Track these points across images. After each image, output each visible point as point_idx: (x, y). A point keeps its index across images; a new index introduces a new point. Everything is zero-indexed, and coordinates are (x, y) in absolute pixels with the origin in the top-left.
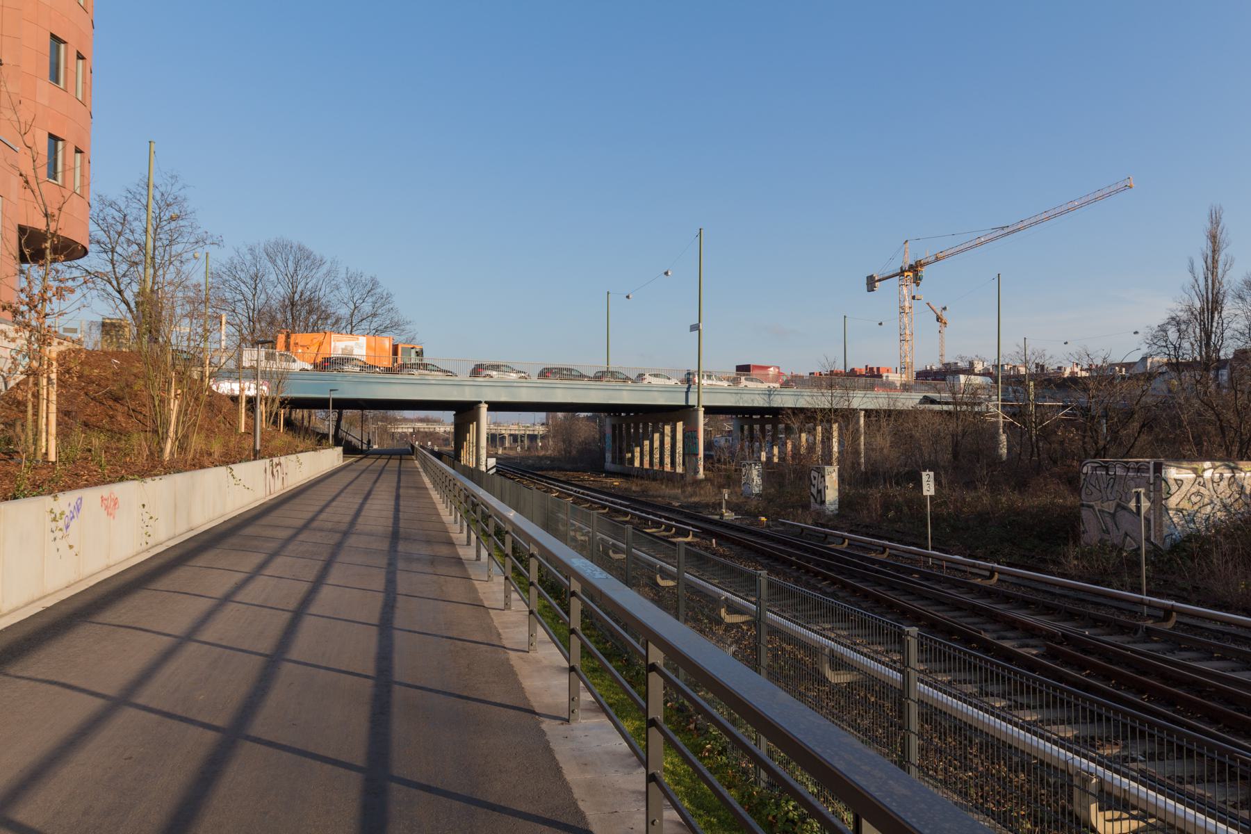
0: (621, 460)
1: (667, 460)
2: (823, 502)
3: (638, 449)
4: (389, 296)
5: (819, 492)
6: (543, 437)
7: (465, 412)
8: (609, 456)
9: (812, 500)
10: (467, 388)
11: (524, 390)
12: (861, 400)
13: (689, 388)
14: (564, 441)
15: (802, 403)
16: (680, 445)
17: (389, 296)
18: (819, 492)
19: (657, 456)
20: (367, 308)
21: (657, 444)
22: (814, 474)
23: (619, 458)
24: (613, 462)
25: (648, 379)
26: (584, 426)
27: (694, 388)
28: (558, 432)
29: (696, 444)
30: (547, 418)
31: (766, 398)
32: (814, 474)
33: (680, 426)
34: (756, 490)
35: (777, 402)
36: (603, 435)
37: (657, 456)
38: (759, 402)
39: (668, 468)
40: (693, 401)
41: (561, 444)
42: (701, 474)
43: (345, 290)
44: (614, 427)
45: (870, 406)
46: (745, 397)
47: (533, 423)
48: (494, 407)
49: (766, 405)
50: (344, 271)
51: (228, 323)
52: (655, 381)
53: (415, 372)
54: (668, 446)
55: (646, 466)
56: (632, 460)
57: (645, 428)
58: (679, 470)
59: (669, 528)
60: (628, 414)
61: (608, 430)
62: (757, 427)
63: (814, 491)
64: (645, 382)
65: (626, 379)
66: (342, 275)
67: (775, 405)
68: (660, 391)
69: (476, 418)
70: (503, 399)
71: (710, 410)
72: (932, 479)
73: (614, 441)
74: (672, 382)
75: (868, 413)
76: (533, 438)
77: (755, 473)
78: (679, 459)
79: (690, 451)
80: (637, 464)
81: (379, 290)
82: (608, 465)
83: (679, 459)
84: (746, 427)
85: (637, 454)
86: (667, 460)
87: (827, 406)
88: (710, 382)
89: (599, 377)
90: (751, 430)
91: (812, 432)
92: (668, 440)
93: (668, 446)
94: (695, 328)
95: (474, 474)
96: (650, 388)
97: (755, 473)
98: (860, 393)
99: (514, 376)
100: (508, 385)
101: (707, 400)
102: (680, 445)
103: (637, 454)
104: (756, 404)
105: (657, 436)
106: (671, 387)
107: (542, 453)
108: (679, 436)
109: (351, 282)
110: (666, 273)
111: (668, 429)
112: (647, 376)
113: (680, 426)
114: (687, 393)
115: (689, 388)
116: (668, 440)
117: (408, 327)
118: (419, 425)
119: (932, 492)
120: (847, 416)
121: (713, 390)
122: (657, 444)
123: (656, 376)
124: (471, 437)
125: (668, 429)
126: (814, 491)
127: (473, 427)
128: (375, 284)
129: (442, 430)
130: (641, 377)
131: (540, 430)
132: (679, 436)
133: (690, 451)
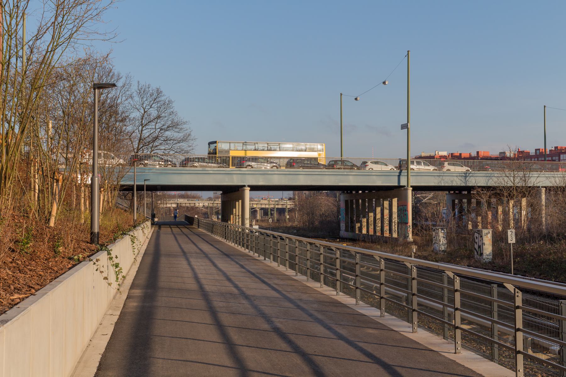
0: (353, 228)
1: (386, 228)
2: (482, 254)
3: (365, 220)
4: (170, 102)
5: (479, 247)
6: (290, 211)
7: (231, 194)
8: (343, 226)
9: (476, 253)
10: (235, 176)
11: (276, 176)
12: (541, 179)
13: (400, 173)
14: (308, 214)
15: (491, 183)
16: (395, 216)
17: (170, 102)
18: (479, 247)
19: (379, 224)
20: (154, 113)
21: (379, 216)
22: (476, 235)
23: (351, 228)
24: (346, 230)
25: (370, 165)
26: (325, 203)
27: (404, 172)
28: (301, 207)
29: (406, 215)
30: (294, 195)
31: (463, 179)
32: (476, 235)
33: (395, 201)
34: (443, 248)
35: (472, 182)
36: (339, 212)
37: (379, 224)
38: (457, 182)
39: (387, 234)
40: (403, 182)
41: (305, 217)
42: (411, 238)
43: (137, 99)
44: (346, 202)
45: (548, 184)
46: (446, 179)
47: (284, 200)
48: (254, 188)
49: (463, 185)
50: (137, 84)
51: (527, 324)
52: (377, 168)
53: (196, 164)
54: (386, 217)
55: (378, 234)
56: (360, 229)
57: (370, 201)
58: (395, 235)
59: (368, 268)
60: (363, 192)
61: (342, 205)
62: (465, 201)
63: (476, 246)
64: (367, 168)
65: (353, 166)
66: (134, 88)
67: (470, 185)
68: (379, 175)
69: (242, 198)
70: (261, 183)
71: (416, 189)
72: (514, 234)
73: (347, 214)
74: (389, 167)
75: (548, 189)
76: (281, 211)
77: (441, 235)
78: (395, 227)
79: (403, 222)
80: (364, 231)
81: (163, 98)
82: (343, 233)
83: (395, 227)
84: (457, 201)
85: (365, 224)
86: (386, 228)
87: (510, 184)
88: (418, 167)
89: (332, 165)
90: (461, 202)
91: (518, 204)
92: (386, 212)
93: (386, 217)
94: (405, 126)
95: (242, 238)
96: (372, 173)
97: (441, 235)
98: (535, 174)
99: (268, 166)
100: (265, 173)
101: (414, 182)
102: (395, 216)
103: (365, 224)
104: (454, 184)
105: (378, 210)
106: (387, 172)
107: (290, 224)
108: (395, 209)
109: (142, 92)
110: (384, 83)
111: (386, 204)
112: (369, 163)
113: (395, 201)
114: (399, 176)
115: (400, 173)
116: (386, 212)
117: (184, 126)
118: (181, 201)
119: (514, 241)
120: (531, 192)
121: (419, 174)
122: (379, 216)
123: (376, 163)
124: (237, 211)
125: (386, 204)
126: (476, 246)
127: (238, 204)
128: (159, 92)
129: (201, 205)
130: (364, 164)
131: (289, 205)
132: (395, 209)
133: (403, 222)
